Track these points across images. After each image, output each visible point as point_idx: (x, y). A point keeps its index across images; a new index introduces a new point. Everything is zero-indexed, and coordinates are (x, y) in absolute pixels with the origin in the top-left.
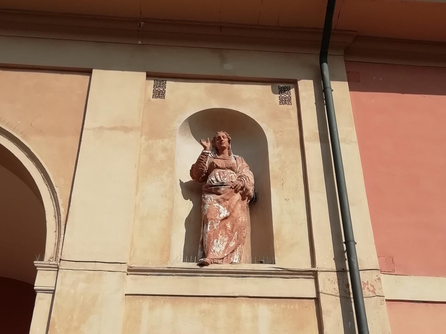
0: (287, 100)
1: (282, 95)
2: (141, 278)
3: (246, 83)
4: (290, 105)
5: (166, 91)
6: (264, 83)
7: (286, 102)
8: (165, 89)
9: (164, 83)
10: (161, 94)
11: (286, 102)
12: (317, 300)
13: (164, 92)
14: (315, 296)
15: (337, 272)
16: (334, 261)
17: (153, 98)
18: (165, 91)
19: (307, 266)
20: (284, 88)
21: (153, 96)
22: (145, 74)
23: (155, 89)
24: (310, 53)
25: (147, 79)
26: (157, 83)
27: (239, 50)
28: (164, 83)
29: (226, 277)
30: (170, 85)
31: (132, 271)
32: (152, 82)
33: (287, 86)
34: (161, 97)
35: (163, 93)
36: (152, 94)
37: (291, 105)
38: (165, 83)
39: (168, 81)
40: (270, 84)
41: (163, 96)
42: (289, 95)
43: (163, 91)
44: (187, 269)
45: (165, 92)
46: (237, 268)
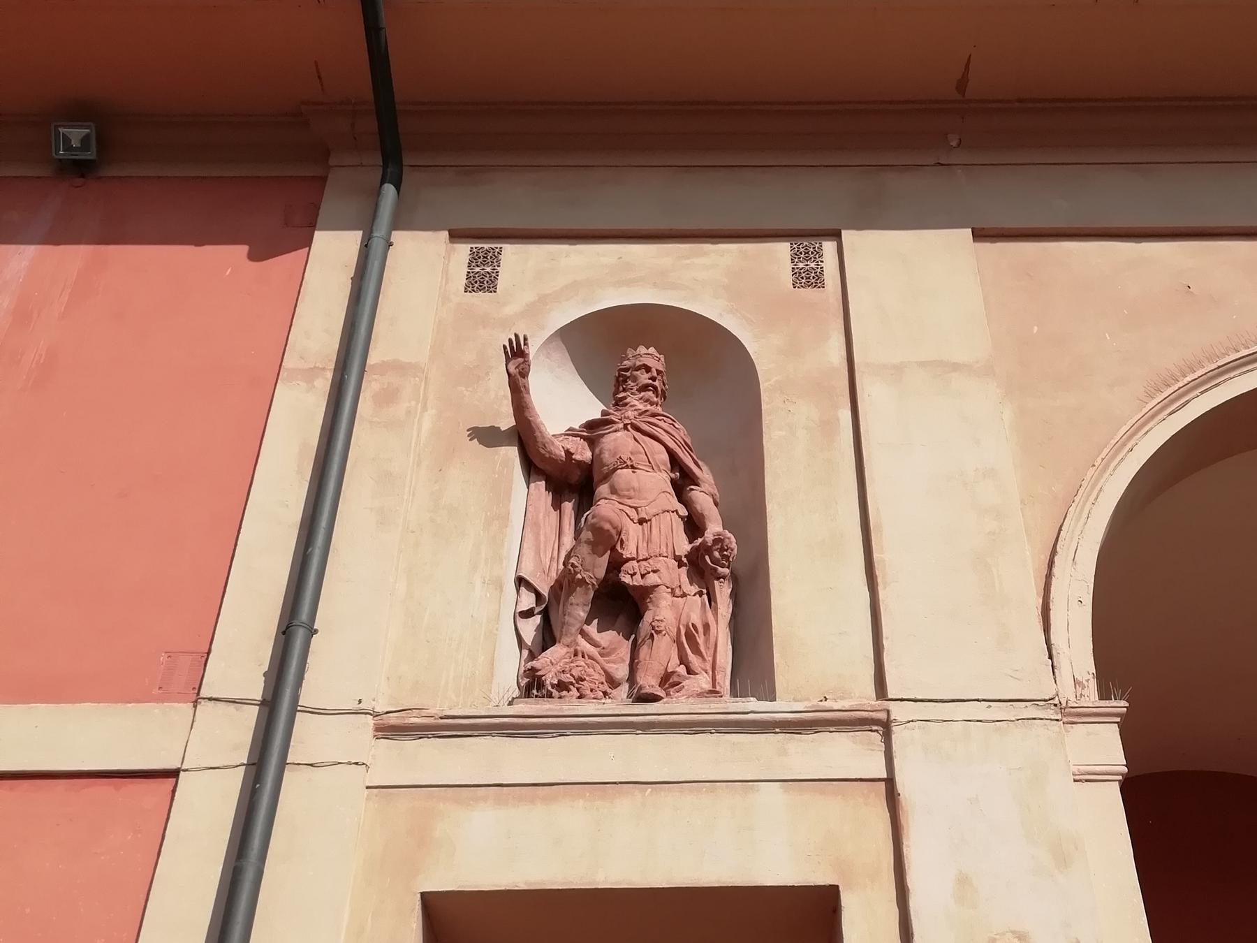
1: (814, 266)
2: (411, 746)
3: (539, 240)
4: (819, 287)
6: (761, 239)
8: (498, 268)
10: (487, 282)
11: (809, 282)
12: (890, 782)
13: (819, 270)
14: (884, 776)
15: (195, 704)
16: (264, 678)
17: (795, 287)
18: (822, 268)
19: (861, 695)
20: (487, 250)
23: (795, 265)
25: (974, 241)
26: (798, 251)
29: (711, 733)
30: (511, 253)
31: (390, 730)
32: (463, 250)
33: (493, 247)
34: (814, 284)
35: (492, 278)
38: (498, 253)
39: (825, 240)
40: (834, 238)
41: (491, 286)
42: (795, 267)
43: (493, 273)
44: (550, 720)
45: (498, 276)
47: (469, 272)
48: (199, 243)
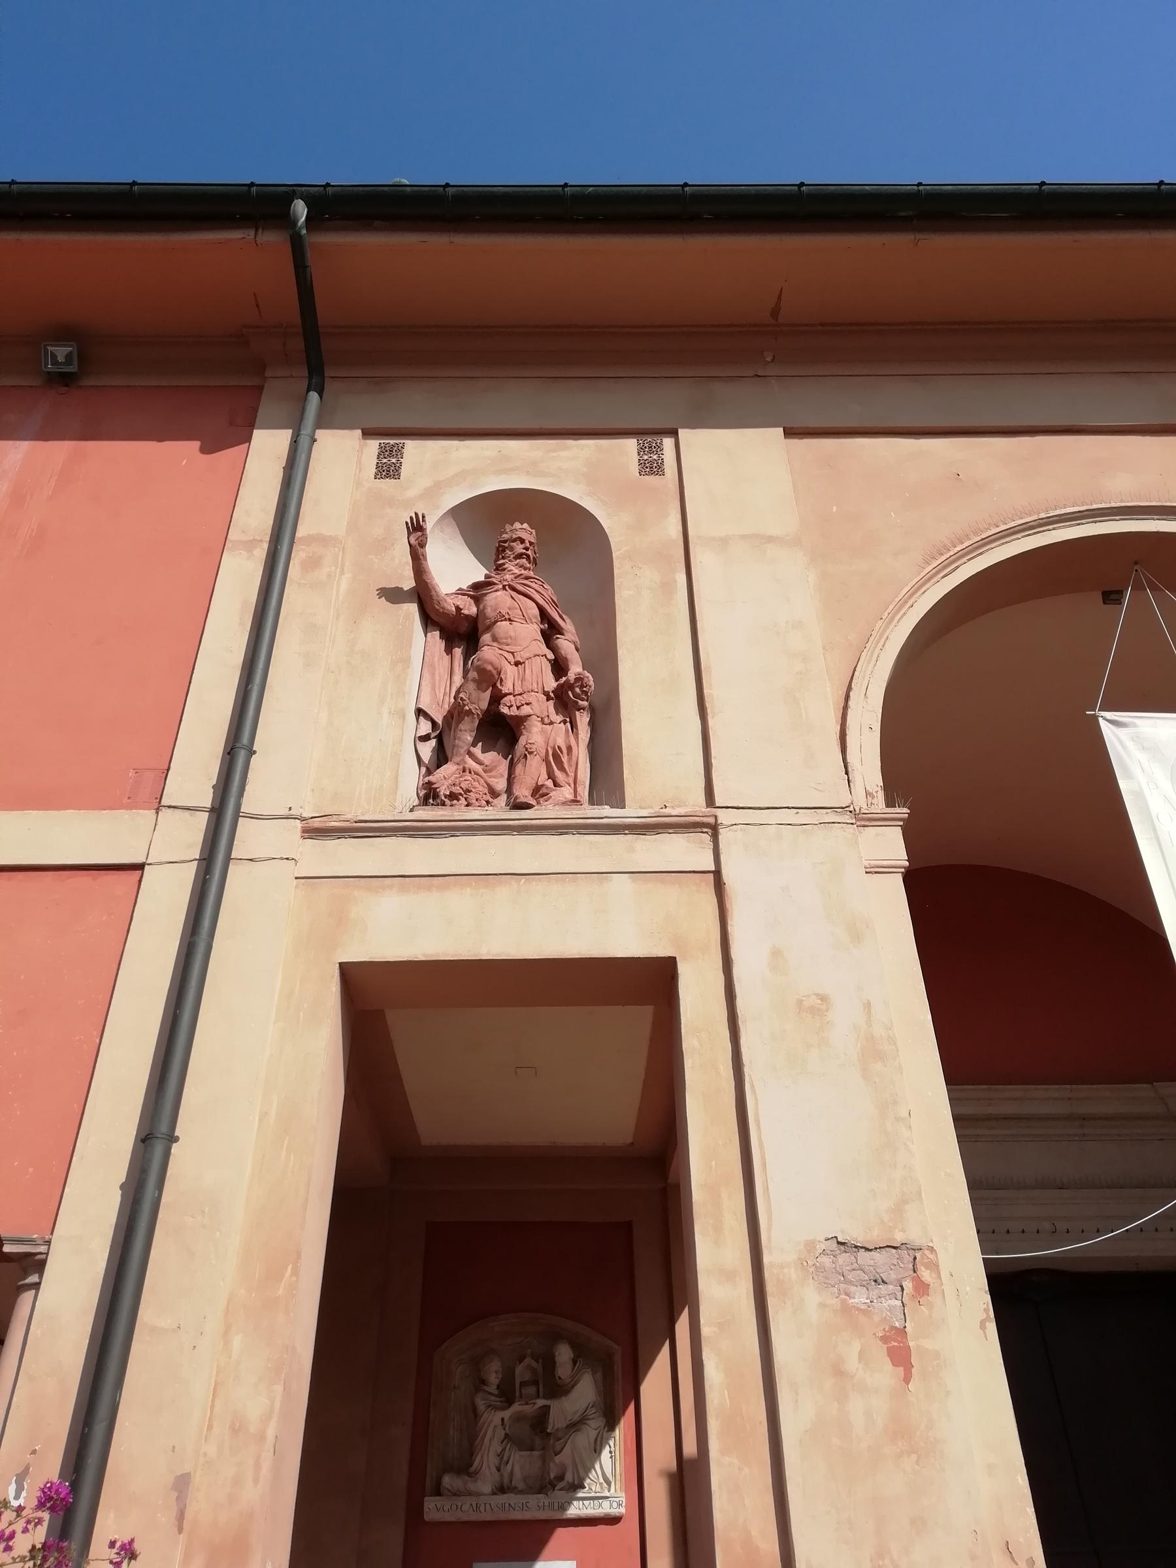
0: (392, 468)
3: (434, 437)
5: (403, 464)
7: (652, 471)
9: (400, 448)
10: (393, 471)
11: (652, 471)
13: (660, 461)
14: (713, 868)
19: (693, 803)
21: (376, 474)
22: (359, 432)
24: (1054, 372)
27: (826, 378)
28: (400, 448)
30: (412, 448)
31: (315, 832)
36: (374, 470)
37: (399, 479)
40: (671, 435)
46: (586, 814)
47: (378, 463)
48: (160, 440)
